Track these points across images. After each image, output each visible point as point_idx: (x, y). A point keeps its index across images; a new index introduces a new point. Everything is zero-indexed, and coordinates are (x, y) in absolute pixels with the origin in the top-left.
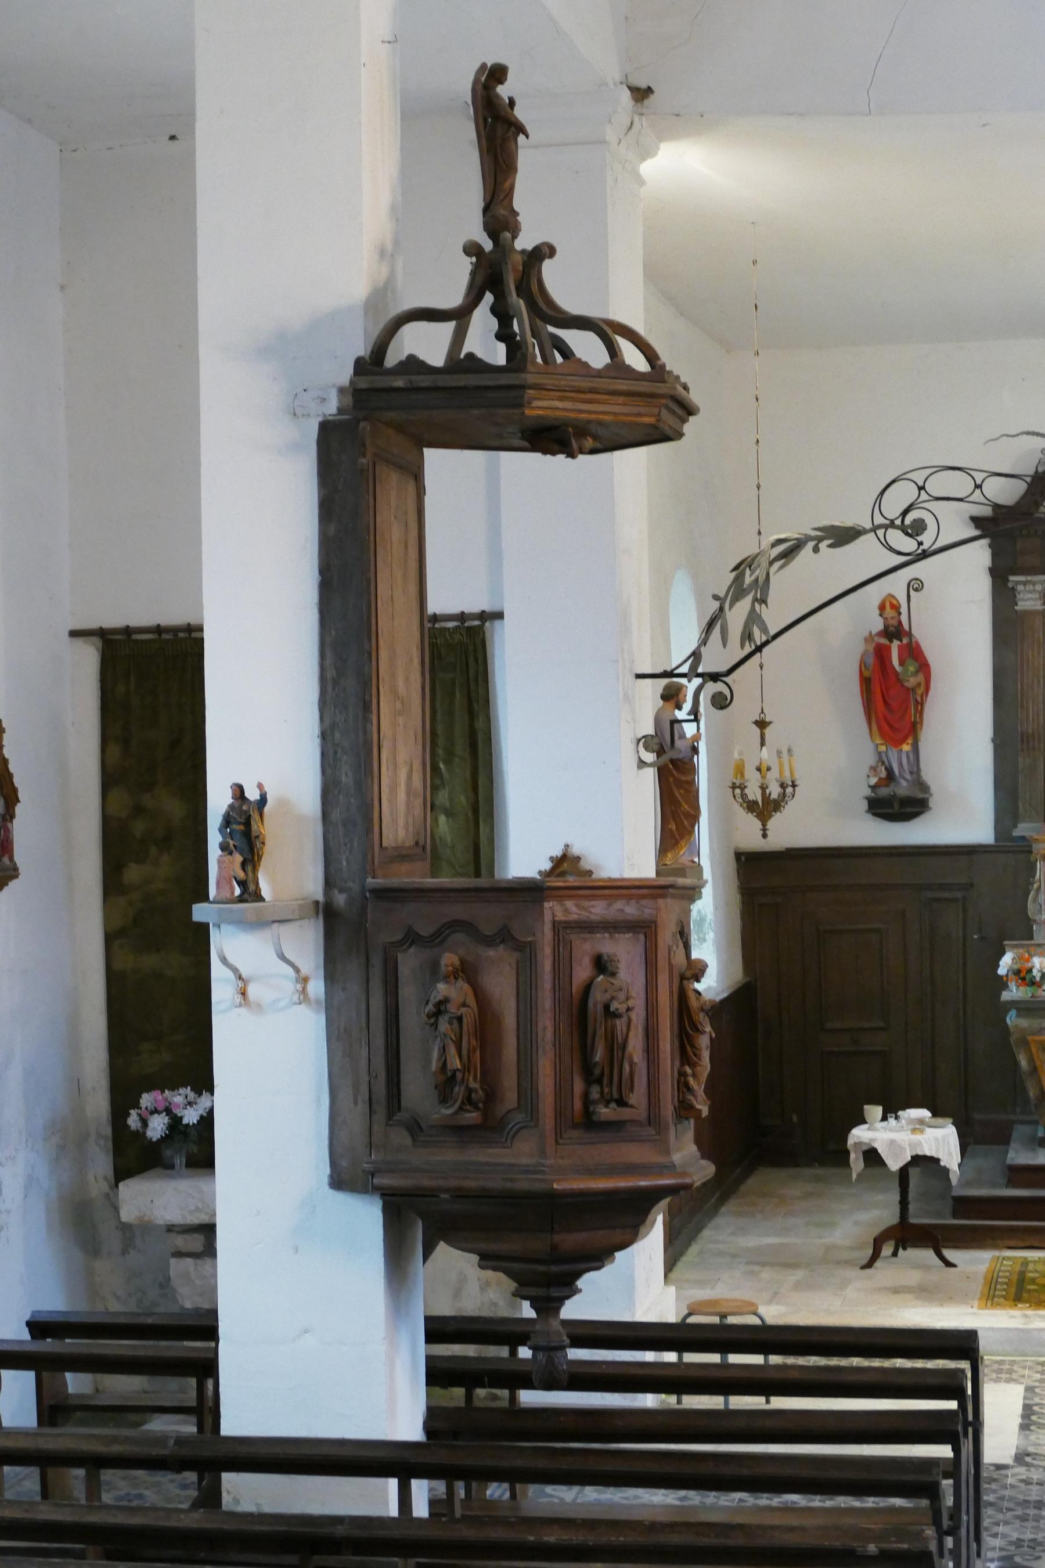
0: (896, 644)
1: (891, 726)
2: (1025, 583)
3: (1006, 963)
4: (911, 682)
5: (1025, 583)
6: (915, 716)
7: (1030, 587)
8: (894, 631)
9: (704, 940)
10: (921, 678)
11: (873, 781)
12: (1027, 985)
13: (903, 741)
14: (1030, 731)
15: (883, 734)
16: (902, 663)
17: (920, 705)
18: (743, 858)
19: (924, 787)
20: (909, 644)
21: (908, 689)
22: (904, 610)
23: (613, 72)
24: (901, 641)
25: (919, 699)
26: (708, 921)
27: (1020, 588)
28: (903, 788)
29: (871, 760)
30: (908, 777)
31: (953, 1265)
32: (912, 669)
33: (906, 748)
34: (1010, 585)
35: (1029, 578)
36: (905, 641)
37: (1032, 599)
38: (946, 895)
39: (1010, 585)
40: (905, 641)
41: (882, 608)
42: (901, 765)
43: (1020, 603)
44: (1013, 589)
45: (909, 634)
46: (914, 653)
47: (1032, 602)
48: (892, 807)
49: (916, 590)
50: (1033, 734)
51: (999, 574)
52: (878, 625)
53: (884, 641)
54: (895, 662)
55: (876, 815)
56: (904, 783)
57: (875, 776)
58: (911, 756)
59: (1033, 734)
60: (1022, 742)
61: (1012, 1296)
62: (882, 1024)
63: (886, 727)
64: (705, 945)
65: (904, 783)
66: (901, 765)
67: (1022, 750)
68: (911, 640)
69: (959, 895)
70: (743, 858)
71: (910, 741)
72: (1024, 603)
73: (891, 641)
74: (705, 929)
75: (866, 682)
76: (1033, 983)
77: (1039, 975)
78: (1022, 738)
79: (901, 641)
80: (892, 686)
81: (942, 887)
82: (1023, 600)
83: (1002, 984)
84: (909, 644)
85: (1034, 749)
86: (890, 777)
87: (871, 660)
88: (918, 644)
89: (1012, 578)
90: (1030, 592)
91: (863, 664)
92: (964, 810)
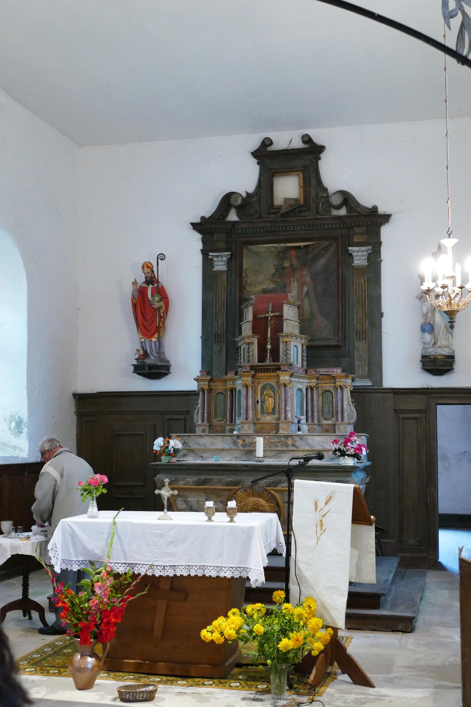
0: (151, 286)
1: (146, 329)
2: (217, 257)
3: (159, 442)
4: (156, 305)
5: (217, 257)
6: (159, 324)
7: (220, 259)
8: (151, 280)
9: (22, 432)
10: (162, 303)
11: (137, 356)
12: (166, 455)
13: (152, 335)
14: (219, 332)
15: (142, 334)
16: (152, 296)
17: (163, 318)
18: (77, 397)
19: (167, 361)
20: (158, 287)
21: (156, 309)
22: (155, 269)
23: (465, 286)
24: (153, 285)
25: (162, 315)
26: (24, 422)
27: (215, 259)
28: (151, 360)
29: (138, 347)
30: (155, 355)
31: (367, 683)
32: (157, 299)
33: (154, 340)
34: (210, 257)
35: (219, 254)
36: (155, 285)
37: (221, 265)
38: (177, 417)
39: (210, 257)
40: (155, 285)
41: (143, 268)
42: (151, 348)
43: (215, 267)
44: (212, 259)
45: (158, 282)
46: (161, 293)
47: (221, 267)
48: (145, 370)
49: (162, 259)
50: (221, 334)
51: (205, 253)
52: (141, 279)
53: (145, 285)
54: (149, 295)
55: (138, 374)
56: (152, 358)
57: (138, 354)
58: (157, 344)
59: (221, 334)
60: (215, 338)
61: (335, 676)
62: (142, 484)
63: (143, 328)
64: (22, 435)
65: (152, 358)
66: (151, 348)
67: (215, 342)
68: (158, 285)
69: (182, 417)
70: (77, 397)
71: (156, 336)
72: (218, 267)
73: (148, 286)
74: (22, 427)
75: (134, 305)
76: (169, 455)
77: (172, 449)
78: (215, 336)
79: (153, 285)
81: (175, 413)
82: (216, 265)
83: (156, 456)
84: (158, 287)
85: (221, 342)
86: (146, 355)
87: (136, 294)
88: (163, 287)
89: (210, 254)
90: (220, 261)
91: (133, 298)
92: (186, 374)
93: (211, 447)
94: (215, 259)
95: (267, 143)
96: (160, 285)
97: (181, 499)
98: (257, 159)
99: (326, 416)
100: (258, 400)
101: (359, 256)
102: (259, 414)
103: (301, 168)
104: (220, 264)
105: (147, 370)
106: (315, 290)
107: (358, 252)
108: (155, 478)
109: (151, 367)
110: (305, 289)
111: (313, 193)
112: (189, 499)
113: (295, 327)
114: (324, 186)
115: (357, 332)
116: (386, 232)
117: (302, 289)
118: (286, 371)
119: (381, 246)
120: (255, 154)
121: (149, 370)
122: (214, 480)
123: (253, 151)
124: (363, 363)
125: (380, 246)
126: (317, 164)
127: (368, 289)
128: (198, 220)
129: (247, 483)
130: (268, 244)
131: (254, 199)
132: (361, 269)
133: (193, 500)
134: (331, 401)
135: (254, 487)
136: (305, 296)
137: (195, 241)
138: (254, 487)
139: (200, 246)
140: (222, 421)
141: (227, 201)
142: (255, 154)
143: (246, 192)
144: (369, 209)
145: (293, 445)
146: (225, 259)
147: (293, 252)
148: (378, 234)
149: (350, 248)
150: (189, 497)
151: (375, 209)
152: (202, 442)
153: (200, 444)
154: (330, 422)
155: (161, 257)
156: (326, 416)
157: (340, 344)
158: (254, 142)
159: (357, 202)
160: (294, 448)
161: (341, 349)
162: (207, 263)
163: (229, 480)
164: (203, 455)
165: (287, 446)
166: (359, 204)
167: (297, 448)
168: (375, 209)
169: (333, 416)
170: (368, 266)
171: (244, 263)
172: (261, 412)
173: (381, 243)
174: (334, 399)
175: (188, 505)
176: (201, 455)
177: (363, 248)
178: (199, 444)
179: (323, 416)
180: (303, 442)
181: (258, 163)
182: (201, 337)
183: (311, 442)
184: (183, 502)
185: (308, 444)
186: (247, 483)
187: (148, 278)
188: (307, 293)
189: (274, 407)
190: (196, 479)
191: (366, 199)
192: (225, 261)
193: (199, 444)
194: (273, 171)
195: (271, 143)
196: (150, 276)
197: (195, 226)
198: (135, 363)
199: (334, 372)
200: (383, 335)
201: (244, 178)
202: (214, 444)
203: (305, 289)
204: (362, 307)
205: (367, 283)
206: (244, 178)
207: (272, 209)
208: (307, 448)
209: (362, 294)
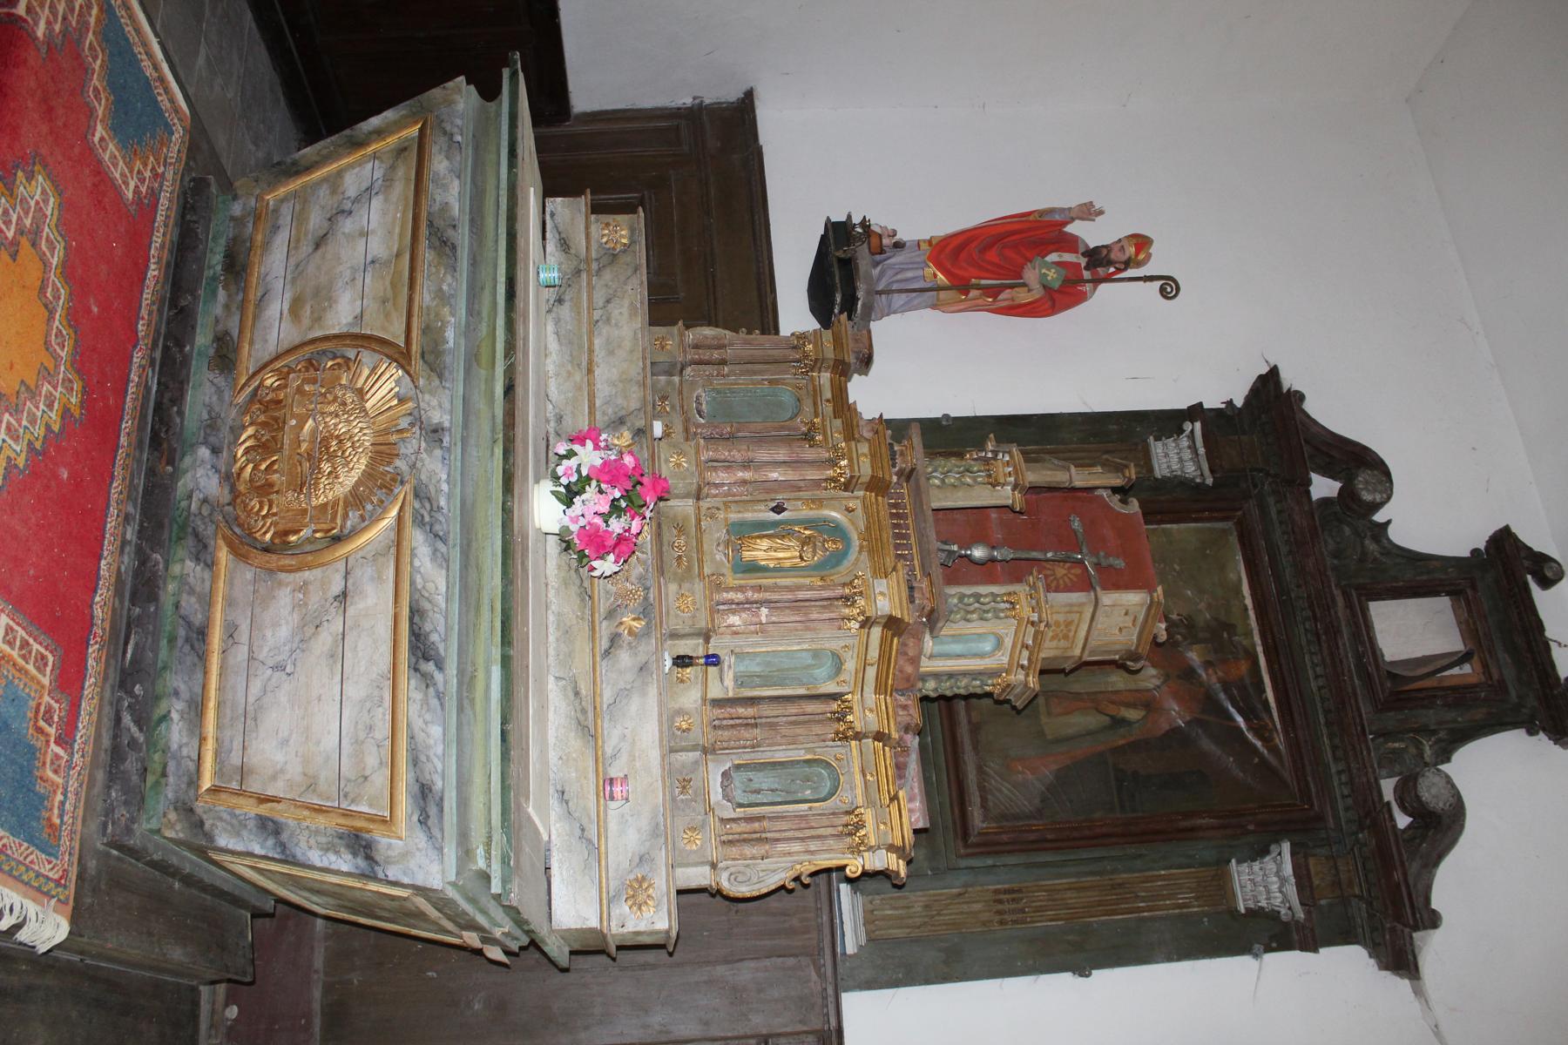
0: (1083, 262)
6: (978, 287)
7: (1187, 455)
8: (1103, 264)
24: (1087, 268)
34: (1188, 426)
35: (1202, 451)
43: (1159, 444)
45: (1097, 281)
48: (837, 249)
49: (1162, 290)
51: (1196, 412)
54: (1053, 257)
55: (824, 239)
68: (1088, 281)
73: (1083, 254)
79: (1087, 268)
80: (1020, 262)
88: (1080, 298)
89: (1198, 425)
93: (597, 342)
94: (1185, 442)
95: (1545, 570)
96: (1088, 287)
97: (378, 174)
98: (1487, 548)
99: (738, 779)
100: (784, 510)
101: (1266, 881)
102: (734, 517)
103: (1496, 676)
104: (1174, 458)
105: (840, 254)
106: (1135, 746)
107: (1278, 874)
108: (462, 78)
109: (848, 265)
110: (1133, 715)
111: (1429, 717)
112: (377, 203)
113: (1063, 643)
114: (1455, 749)
115: (1020, 891)
116: (1348, 964)
117: (1133, 706)
118: (911, 600)
119: (1302, 950)
120: (1504, 540)
121: (840, 260)
122: (449, 279)
123: (1514, 530)
124: (918, 921)
125: (1304, 948)
126: (1514, 725)
127: (1161, 918)
128: (1289, 380)
129: (434, 402)
130: (1254, 595)
131: (1371, 546)
132: (1220, 886)
133: (375, 216)
134: (800, 796)
135: (416, 429)
136: (1112, 717)
137: (1225, 388)
138: (416, 429)
139: (1213, 402)
140: (699, 413)
141: (1357, 462)
142: (1504, 540)
143: (1389, 522)
144: (1428, 900)
145: (614, 639)
146: (1190, 469)
147: (1244, 667)
148: (1344, 937)
149: (1286, 847)
150: (386, 200)
151: (1433, 920)
152: (616, 312)
153: (610, 306)
154: (716, 794)
155: (1169, 288)
156: (738, 779)
157: (972, 839)
158: (1536, 537)
159: (1440, 857)
160: (605, 644)
161: (960, 843)
162: (1168, 422)
163: (450, 334)
164: (567, 305)
165: (611, 614)
166: (1436, 864)
167: (607, 653)
168: (1433, 920)
169: (741, 805)
170: (1233, 912)
171: (1183, 526)
172: (742, 524)
173: (1315, 950)
174: (805, 806)
175: (357, 200)
176: (567, 297)
177: (1292, 890)
178: (608, 301)
179: (738, 767)
180: (629, 677)
181: (1475, 552)
182: (946, 416)
183: (634, 705)
184: (365, 185)
185: (623, 694)
186: (434, 402)
187: (1105, 252)
188: (1118, 722)
189: (765, 569)
190: (456, 212)
191: (1450, 885)
192: (1182, 469)
193: (608, 301)
194: (1469, 592)
195: (1546, 583)
196: (1113, 256)
197: (1269, 381)
198: (856, 220)
199: (911, 800)
200: (998, 981)
201: (1429, 515)
202: (611, 353)
203: (1133, 715)
204: (1100, 903)
205: (1181, 915)
206: (1429, 515)
207: (1359, 596)
208: (607, 695)
209: (1143, 900)
